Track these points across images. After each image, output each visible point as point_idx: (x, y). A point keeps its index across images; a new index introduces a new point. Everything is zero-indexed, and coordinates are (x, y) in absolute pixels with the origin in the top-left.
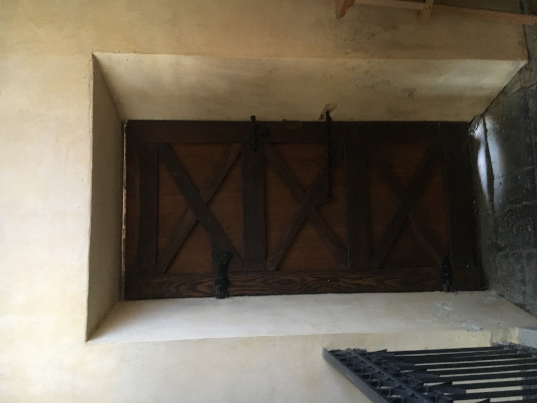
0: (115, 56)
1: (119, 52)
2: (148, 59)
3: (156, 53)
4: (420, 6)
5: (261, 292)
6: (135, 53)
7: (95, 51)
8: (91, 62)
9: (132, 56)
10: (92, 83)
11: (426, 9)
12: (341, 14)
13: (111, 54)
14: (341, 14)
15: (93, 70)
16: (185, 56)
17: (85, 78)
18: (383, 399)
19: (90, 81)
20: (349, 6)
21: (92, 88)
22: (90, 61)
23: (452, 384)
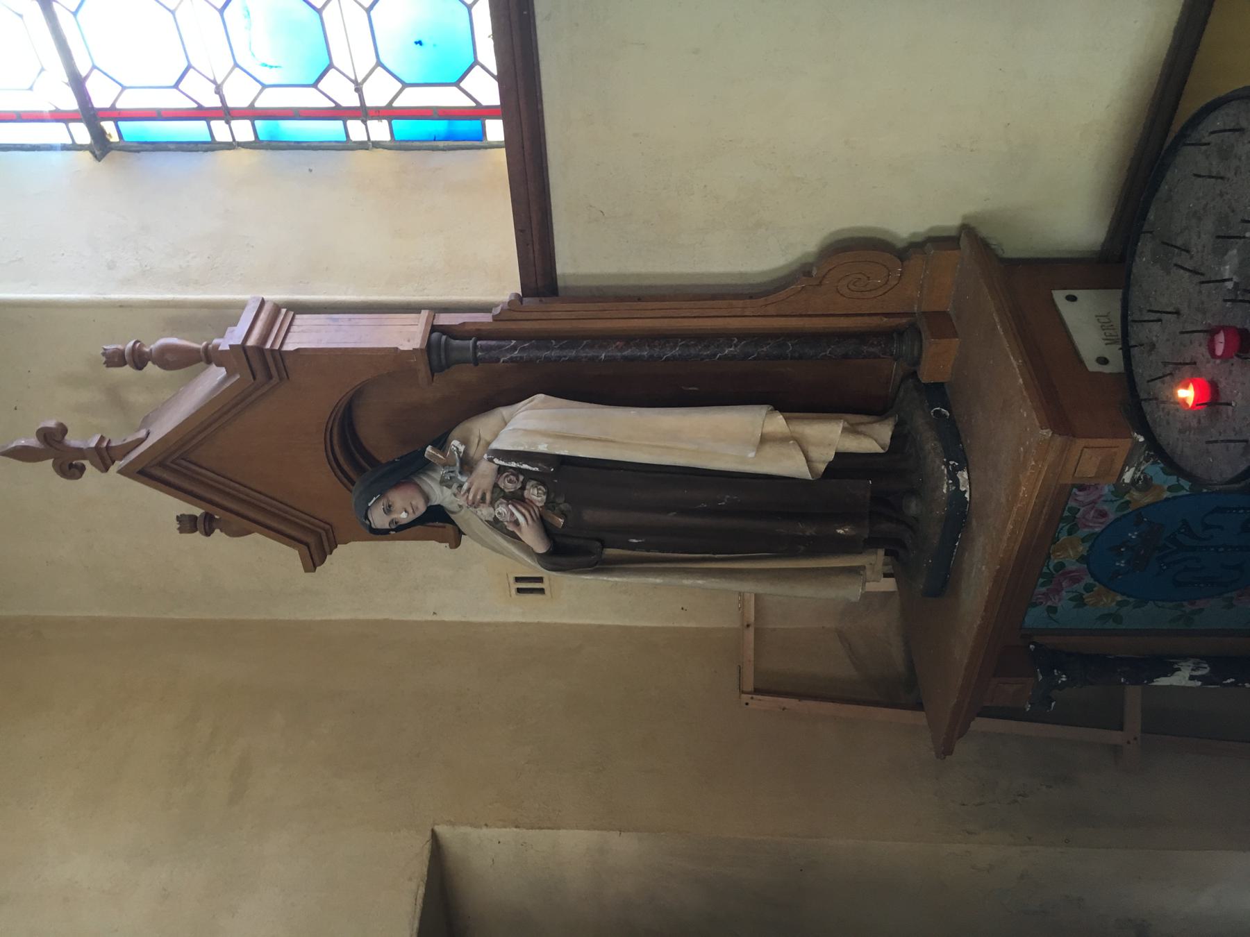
0: (474, 834)
1: (486, 825)
2: (540, 839)
3: (559, 828)
4: (1115, 737)
5: (185, 145)
6: (516, 827)
7: (438, 825)
8: (428, 846)
9: (509, 833)
10: (422, 891)
11: (1129, 743)
12: (946, 750)
13: (468, 830)
14: (946, 750)
15: (427, 863)
16: (619, 833)
17: (410, 879)
18: (743, 269)
19: (418, 886)
20: (960, 736)
21: (420, 901)
22: (426, 844)
23: (240, 374)
